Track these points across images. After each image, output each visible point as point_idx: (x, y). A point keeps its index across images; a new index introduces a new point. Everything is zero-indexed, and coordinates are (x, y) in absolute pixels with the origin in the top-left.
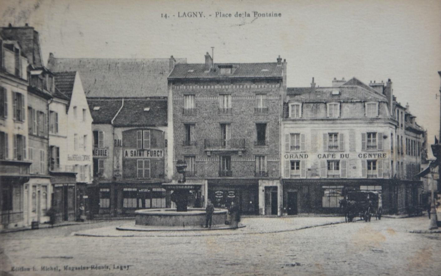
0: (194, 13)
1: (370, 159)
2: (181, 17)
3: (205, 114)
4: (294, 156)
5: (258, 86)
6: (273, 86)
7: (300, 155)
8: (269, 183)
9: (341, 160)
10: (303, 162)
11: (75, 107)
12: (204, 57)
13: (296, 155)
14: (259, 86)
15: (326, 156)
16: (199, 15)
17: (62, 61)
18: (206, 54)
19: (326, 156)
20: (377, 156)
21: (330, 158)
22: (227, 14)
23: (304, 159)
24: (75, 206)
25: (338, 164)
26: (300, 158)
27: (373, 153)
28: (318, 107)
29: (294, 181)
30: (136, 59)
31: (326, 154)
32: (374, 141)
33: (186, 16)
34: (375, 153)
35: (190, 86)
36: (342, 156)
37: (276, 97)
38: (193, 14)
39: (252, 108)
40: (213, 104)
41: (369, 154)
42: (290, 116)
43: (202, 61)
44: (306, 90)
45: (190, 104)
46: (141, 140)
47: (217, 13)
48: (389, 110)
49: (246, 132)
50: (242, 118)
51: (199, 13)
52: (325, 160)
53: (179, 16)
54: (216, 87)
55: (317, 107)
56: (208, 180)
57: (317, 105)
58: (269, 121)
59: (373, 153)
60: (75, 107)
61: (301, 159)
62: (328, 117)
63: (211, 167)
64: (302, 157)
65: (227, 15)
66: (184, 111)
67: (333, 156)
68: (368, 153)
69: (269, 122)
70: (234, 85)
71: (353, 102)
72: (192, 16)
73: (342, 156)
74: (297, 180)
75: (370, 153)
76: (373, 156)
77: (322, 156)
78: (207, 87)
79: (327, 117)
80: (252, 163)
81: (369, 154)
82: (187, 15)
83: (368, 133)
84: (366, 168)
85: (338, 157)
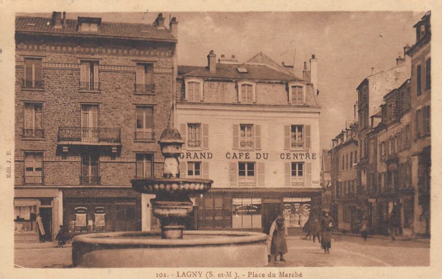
10: (309, 164)
13: (195, 154)
15: (238, 156)
19: (238, 156)
20: (304, 157)
23: (207, 160)
27: (299, 153)
47: (250, 273)
52: (236, 161)
53: (178, 276)
59: (299, 153)
61: (203, 160)
63: (68, 170)
67: (246, 155)
69: (156, 105)
75: (295, 153)
76: (299, 157)
77: (232, 155)
81: (294, 154)
82: (186, 275)
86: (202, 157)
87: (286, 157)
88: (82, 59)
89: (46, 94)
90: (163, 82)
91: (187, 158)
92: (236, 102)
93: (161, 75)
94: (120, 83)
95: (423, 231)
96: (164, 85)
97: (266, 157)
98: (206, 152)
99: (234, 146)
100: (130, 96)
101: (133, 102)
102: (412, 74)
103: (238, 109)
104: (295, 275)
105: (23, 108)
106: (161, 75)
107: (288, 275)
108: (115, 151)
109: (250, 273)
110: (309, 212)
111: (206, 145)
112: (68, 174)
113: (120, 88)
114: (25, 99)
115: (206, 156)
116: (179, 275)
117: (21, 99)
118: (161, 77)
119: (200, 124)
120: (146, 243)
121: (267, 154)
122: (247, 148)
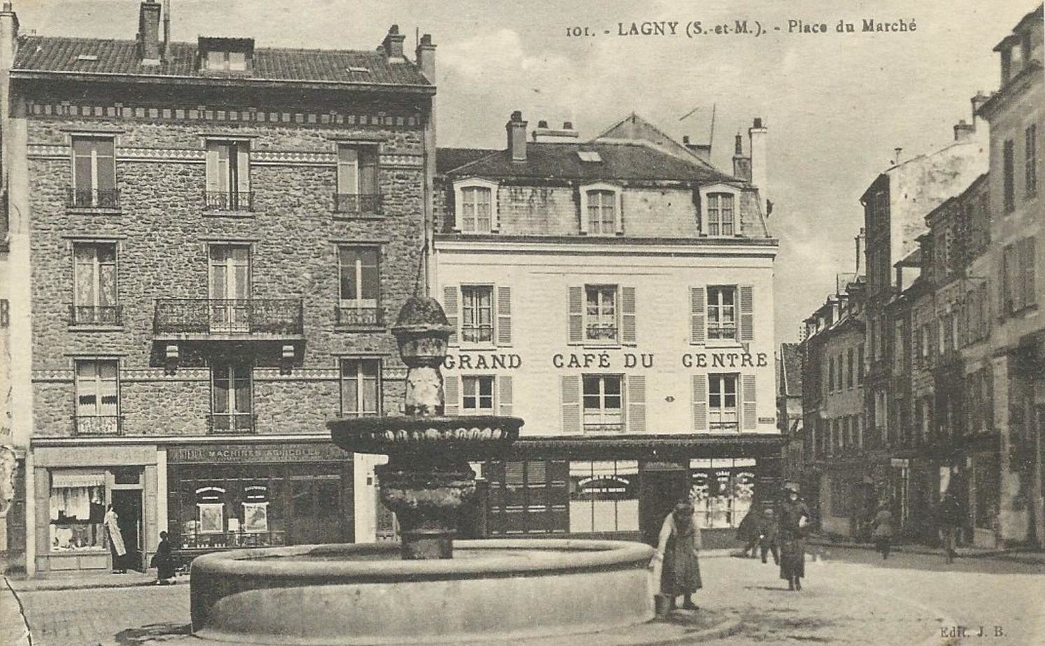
0: (657, 26)
1: (720, 370)
2: (627, 34)
3: (153, 210)
4: (474, 363)
7: (495, 357)
8: (944, 476)
9: (629, 372)
15: (582, 361)
16: (667, 28)
19: (582, 361)
21: (594, 369)
22: (817, 25)
25: (730, 387)
26: (494, 367)
27: (725, 352)
28: (549, 198)
29: (736, 441)
31: (579, 352)
32: (730, 313)
33: (637, 33)
34: (732, 351)
36: (631, 358)
38: (653, 27)
39: (325, 195)
41: (715, 356)
42: (459, 225)
44: (882, 228)
46: (477, 232)
47: (793, 24)
50: (289, 227)
51: (670, 24)
53: (620, 34)
55: (544, 198)
56: (168, 446)
57: (545, 191)
58: (385, 239)
59: (725, 352)
61: (499, 372)
62: (585, 234)
64: (502, 365)
65: (816, 28)
68: (709, 353)
71: (661, 187)
72: (653, 32)
73: (631, 358)
74: (732, 437)
75: (718, 352)
76: (727, 362)
77: (567, 361)
79: (580, 233)
80: (328, 383)
83: (709, 288)
85: (616, 366)
86: (500, 358)
87: (695, 361)
91: (461, 367)
92: (574, 233)
93: (398, 172)
94: (299, 194)
97: (647, 363)
98: (506, 351)
99: (572, 338)
100: (325, 224)
103: (638, 250)
104: (899, 27)
106: (398, 172)
107: (884, 28)
109: (793, 24)
111: (506, 337)
112: (179, 410)
115: (507, 363)
116: (624, 32)
121: (651, 356)
122: (605, 341)
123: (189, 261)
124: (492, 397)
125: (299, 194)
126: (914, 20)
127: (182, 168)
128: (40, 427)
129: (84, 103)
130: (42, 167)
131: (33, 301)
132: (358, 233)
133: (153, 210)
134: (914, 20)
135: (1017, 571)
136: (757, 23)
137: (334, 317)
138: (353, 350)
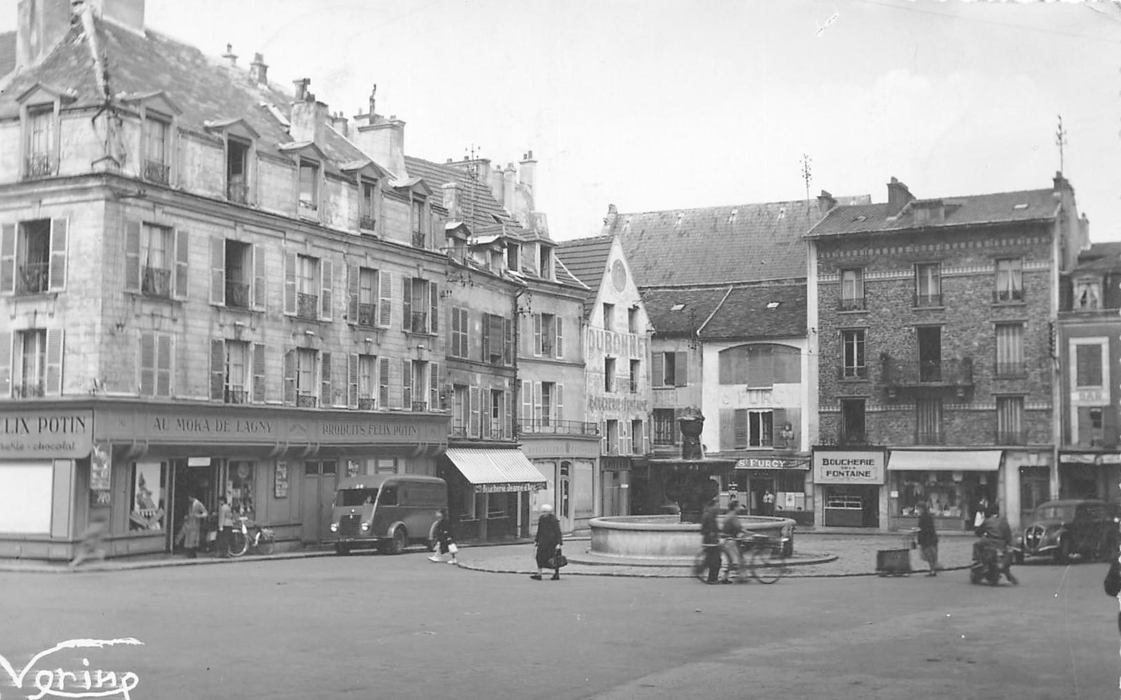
5: (1032, 241)
6: (1036, 240)
8: (1028, 459)
11: (608, 307)
12: (887, 187)
14: (1004, 243)
17: (630, 219)
18: (1054, 176)
24: (170, 532)
30: (349, 219)
35: (928, 245)
37: (965, 269)
40: (903, 288)
43: (881, 196)
45: (851, 292)
48: (1092, 295)
49: (976, 344)
54: (908, 249)
58: (1026, 318)
60: (608, 307)
63: (899, 423)
66: (841, 306)
69: (1027, 321)
70: (841, 250)
78: (889, 251)
84: (187, 537)
88: (512, 325)
89: (869, 316)
90: (1038, 285)
93: (1034, 274)
94: (971, 292)
95: (420, 184)
96: (1039, 288)
100: (987, 311)
101: (991, 319)
102: (933, 205)
105: (327, 344)
106: (1034, 274)
108: (893, 396)
110: (536, 548)
112: (899, 430)
113: (971, 300)
114: (843, 325)
117: (837, 326)
118: (1036, 277)
119: (250, 342)
120: (424, 388)
123: (906, 338)
124: (761, 411)
125: (971, 292)
126: (229, 46)
127: (901, 282)
128: (822, 439)
129: (884, 247)
130: (825, 289)
131: (820, 366)
132: (1008, 315)
133: (884, 310)
134: (229, 46)
135: (32, 535)
136: (375, 86)
137: (993, 370)
138: (1005, 391)
